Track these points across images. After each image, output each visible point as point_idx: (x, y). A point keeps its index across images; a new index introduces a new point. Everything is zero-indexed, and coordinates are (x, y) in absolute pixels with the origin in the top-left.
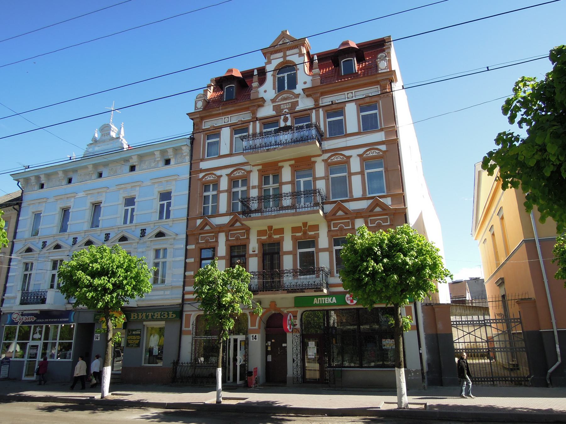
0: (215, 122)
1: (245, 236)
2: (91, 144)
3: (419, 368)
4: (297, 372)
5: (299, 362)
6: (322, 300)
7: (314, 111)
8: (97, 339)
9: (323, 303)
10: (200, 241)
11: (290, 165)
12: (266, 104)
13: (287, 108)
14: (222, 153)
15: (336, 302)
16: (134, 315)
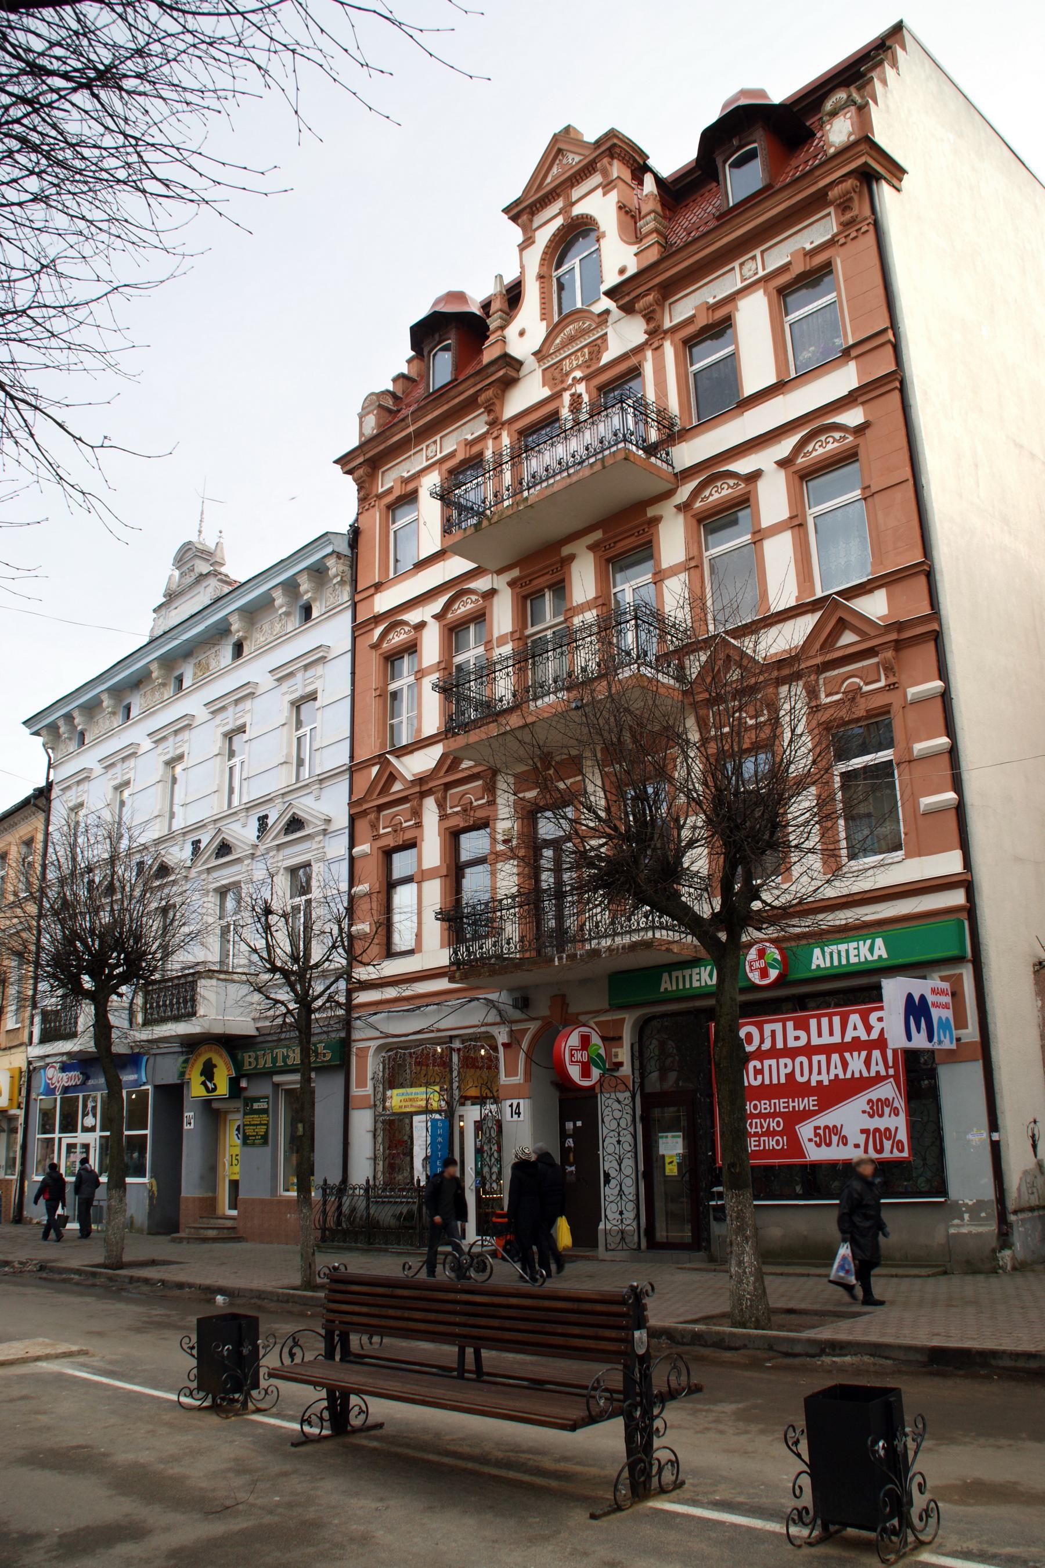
0: (406, 465)
1: (878, 680)
2: (160, 607)
3: (989, 1193)
4: (621, 1213)
5: (629, 1182)
6: (839, 953)
7: (649, 354)
8: (188, 1127)
9: (844, 962)
10: (382, 831)
11: (591, 548)
12: (524, 370)
13: (578, 367)
14: (750, 386)
15: (885, 956)
16: (250, 1057)
